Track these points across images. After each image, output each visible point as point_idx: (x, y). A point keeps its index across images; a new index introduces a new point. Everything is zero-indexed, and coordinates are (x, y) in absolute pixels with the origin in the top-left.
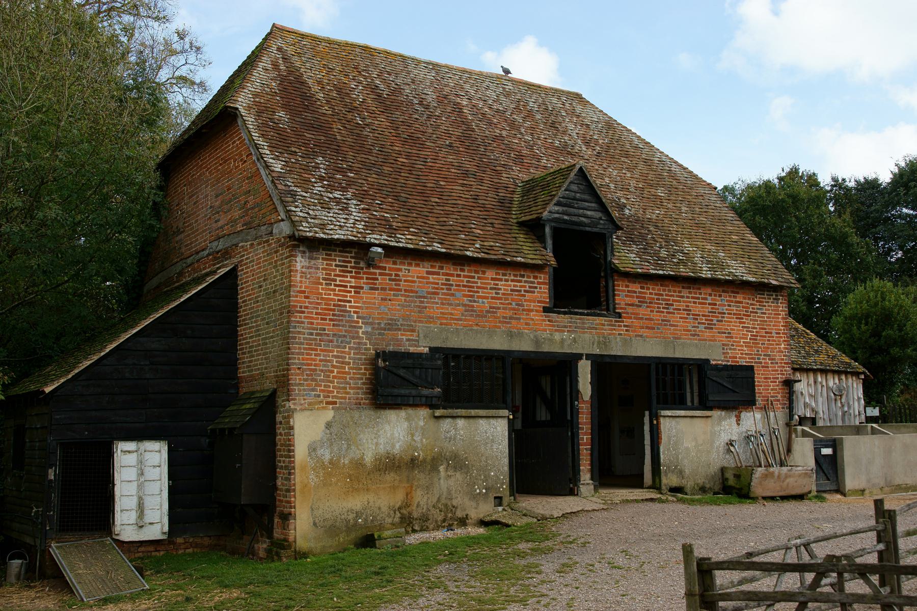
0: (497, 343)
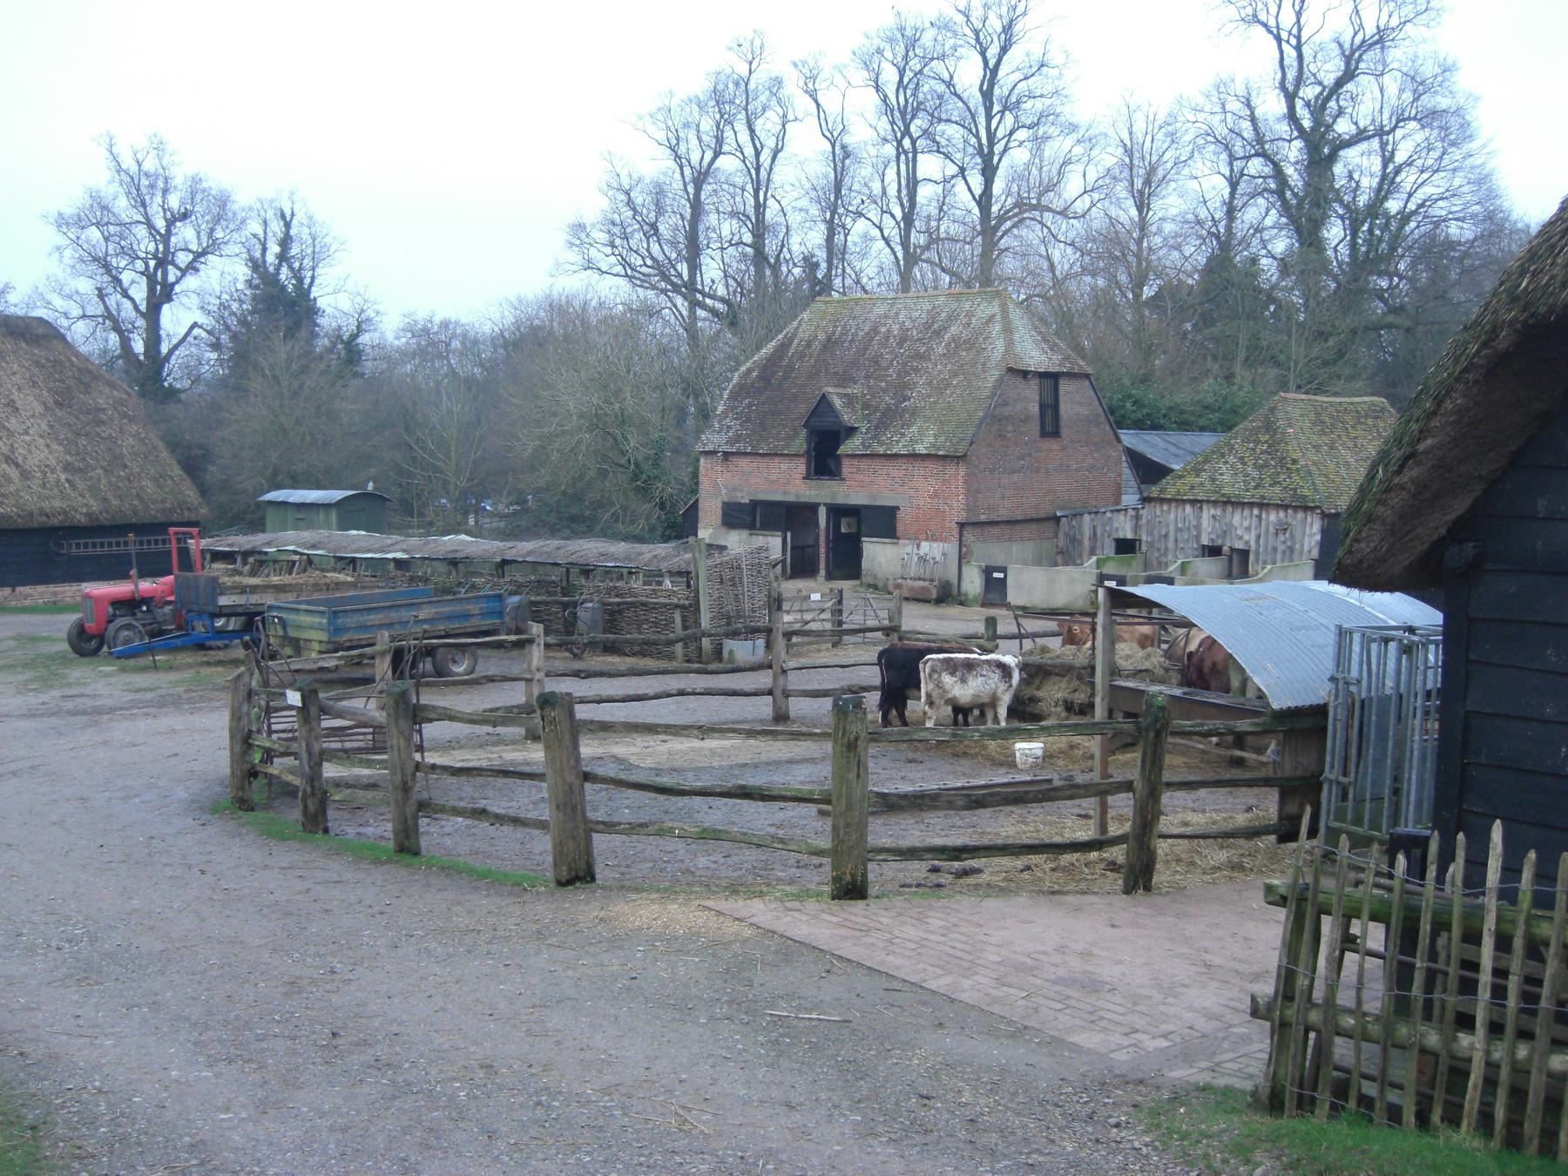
0: (778, 498)
